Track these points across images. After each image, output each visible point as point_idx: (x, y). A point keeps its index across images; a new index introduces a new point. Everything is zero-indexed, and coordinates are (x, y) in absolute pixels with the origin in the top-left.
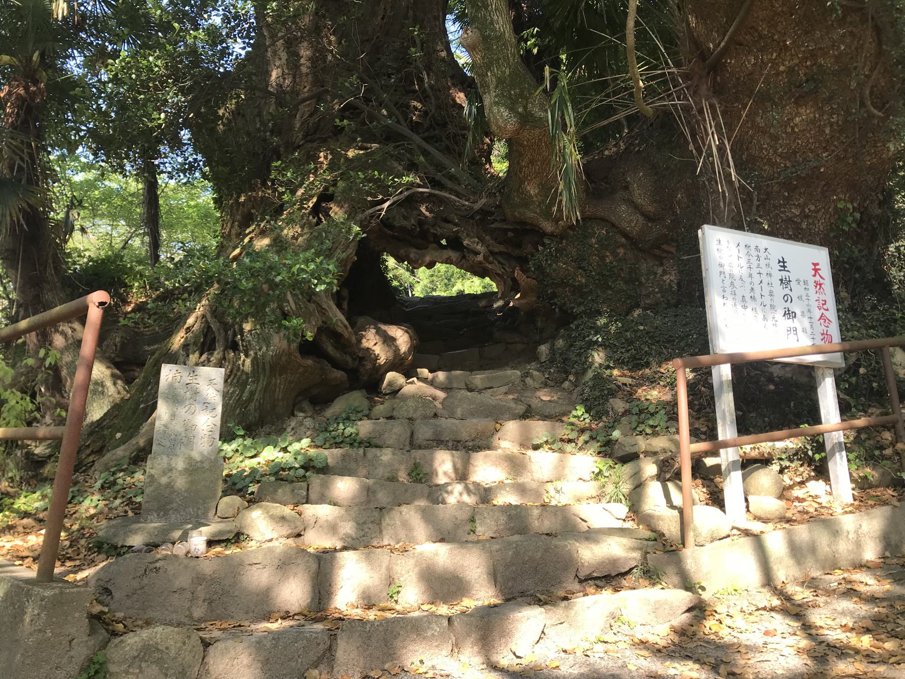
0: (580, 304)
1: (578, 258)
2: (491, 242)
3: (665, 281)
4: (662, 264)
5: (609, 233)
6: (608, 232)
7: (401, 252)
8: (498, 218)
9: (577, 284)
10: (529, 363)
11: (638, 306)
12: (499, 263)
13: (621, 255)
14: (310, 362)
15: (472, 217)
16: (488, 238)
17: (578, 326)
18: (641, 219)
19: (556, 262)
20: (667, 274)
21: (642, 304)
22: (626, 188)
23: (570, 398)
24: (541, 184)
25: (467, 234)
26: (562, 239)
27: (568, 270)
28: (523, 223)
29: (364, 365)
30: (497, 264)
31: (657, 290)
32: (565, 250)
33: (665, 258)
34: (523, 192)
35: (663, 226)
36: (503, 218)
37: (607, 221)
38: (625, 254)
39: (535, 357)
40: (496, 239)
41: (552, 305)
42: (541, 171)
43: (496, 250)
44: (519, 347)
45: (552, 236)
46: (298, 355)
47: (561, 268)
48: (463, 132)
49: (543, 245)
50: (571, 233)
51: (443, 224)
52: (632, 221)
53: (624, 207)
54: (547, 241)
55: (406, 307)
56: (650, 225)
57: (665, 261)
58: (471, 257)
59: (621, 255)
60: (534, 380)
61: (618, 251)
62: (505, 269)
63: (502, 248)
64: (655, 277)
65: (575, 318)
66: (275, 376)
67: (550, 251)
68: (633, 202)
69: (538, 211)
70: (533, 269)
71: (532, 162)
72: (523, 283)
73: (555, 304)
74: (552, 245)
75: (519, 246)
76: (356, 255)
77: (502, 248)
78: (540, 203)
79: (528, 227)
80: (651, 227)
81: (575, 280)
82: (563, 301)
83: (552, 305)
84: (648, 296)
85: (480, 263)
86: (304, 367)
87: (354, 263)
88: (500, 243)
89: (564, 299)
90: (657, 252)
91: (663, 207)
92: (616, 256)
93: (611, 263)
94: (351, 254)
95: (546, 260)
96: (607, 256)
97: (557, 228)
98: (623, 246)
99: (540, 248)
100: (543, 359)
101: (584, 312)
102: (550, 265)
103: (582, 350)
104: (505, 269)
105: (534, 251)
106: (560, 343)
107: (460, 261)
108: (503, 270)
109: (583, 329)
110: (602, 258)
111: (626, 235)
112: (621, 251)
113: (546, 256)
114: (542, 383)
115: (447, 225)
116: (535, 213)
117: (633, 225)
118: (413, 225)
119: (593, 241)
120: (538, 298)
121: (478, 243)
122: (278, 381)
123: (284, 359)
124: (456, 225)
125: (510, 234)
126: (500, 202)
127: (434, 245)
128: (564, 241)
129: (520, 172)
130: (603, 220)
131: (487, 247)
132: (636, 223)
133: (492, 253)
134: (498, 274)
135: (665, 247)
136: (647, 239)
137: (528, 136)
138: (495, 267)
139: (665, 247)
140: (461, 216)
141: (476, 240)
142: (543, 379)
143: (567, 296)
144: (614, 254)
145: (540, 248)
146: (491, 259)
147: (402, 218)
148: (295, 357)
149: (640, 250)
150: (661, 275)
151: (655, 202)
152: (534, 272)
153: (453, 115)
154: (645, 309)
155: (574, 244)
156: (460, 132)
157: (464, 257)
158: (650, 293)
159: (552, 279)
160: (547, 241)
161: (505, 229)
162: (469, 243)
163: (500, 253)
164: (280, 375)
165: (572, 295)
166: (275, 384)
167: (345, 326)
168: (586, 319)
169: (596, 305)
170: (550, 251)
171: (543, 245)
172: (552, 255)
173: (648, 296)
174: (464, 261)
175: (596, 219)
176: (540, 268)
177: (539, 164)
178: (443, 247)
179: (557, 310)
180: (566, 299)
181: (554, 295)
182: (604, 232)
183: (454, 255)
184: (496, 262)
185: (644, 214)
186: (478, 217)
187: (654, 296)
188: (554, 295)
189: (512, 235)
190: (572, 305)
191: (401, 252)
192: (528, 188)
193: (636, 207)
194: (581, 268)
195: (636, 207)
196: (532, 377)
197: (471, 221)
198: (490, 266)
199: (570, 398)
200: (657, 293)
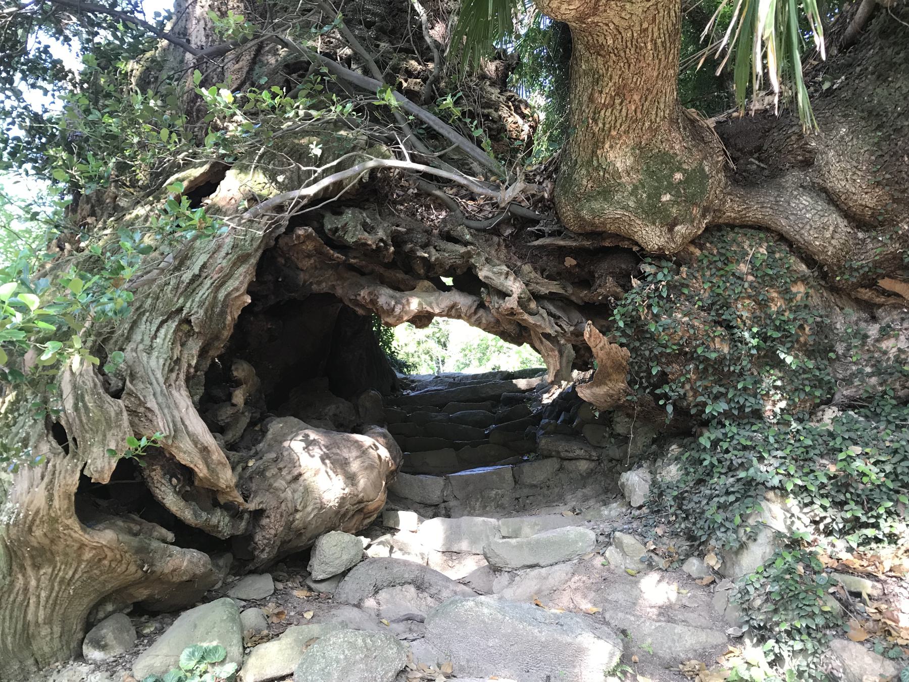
0: (717, 398)
1: (713, 304)
2: (533, 275)
3: (885, 353)
4: (874, 319)
5: (774, 252)
6: (771, 252)
7: (362, 293)
8: (546, 229)
9: (713, 356)
10: (605, 503)
11: (828, 402)
12: (550, 314)
13: (799, 297)
14: (106, 536)
15: (496, 231)
16: (527, 268)
17: (715, 443)
18: (842, 223)
19: (669, 312)
20: (889, 337)
21: (838, 397)
22: (807, 163)
23: (710, 606)
24: (638, 146)
25: (487, 259)
26: (679, 264)
27: (693, 327)
28: (596, 234)
29: (263, 528)
30: (545, 315)
31: (868, 370)
32: (687, 286)
33: (880, 306)
34: (600, 165)
35: (891, 238)
36: (556, 228)
37: (768, 229)
38: (807, 295)
39: (618, 493)
40: (543, 271)
41: (658, 397)
42: (639, 114)
43: (544, 290)
44: (583, 466)
45: (659, 257)
46: (73, 522)
47: (680, 323)
48: (486, 111)
49: (642, 277)
50: (698, 252)
51: (443, 244)
52: (825, 227)
53: (805, 200)
54: (648, 269)
55: (413, 389)
56: (860, 235)
57: (880, 312)
58: (494, 302)
59: (799, 297)
60: (624, 554)
61: (794, 289)
62: (560, 326)
63: (554, 287)
64: (864, 344)
65: (706, 424)
66: (22, 568)
67: (657, 289)
68: (824, 190)
69: (631, 204)
70: (621, 324)
71: (621, 92)
72: (601, 354)
73: (666, 396)
74: (660, 276)
75: (586, 282)
76: (249, 292)
77: (554, 287)
78: (636, 188)
79: (607, 244)
80: (864, 241)
81: (708, 347)
82: (682, 392)
83: (658, 397)
84: (848, 381)
85: (512, 312)
86: (95, 548)
87: (246, 310)
88: (550, 278)
89: (683, 387)
90: (866, 294)
91: (897, 195)
92: (791, 300)
93: (780, 313)
94: (237, 289)
95: (649, 307)
96: (773, 300)
97: (672, 239)
98: (804, 279)
99: (635, 282)
100: (637, 500)
101: (727, 414)
102: (656, 317)
103: (732, 498)
104: (560, 326)
105: (619, 290)
106: (672, 472)
107: (475, 312)
108: (558, 329)
109: (727, 451)
110: (763, 305)
111: (809, 259)
112: (799, 289)
113: (649, 297)
114: (642, 561)
115: (450, 246)
116: (626, 208)
117: (828, 235)
118: (381, 240)
119: (744, 268)
120: (631, 383)
121: (507, 274)
122: (33, 583)
123: (38, 532)
124: (466, 244)
125: (570, 262)
126: (552, 193)
127: (427, 283)
128: (684, 269)
129: (595, 121)
130: (760, 228)
131: (527, 285)
132: (835, 231)
133: (537, 297)
134: (547, 336)
135: (885, 284)
136: (856, 264)
137: (617, 20)
138: (541, 321)
139: (885, 284)
140: (478, 230)
141: (504, 268)
142: (644, 553)
143: (688, 380)
144: (786, 292)
145: (635, 282)
146: (533, 305)
147: (359, 227)
148: (67, 527)
149: (834, 289)
150: (877, 340)
151: (878, 184)
152: (623, 332)
153: (470, 87)
154: (844, 408)
155: (703, 275)
156: (480, 111)
157: (482, 305)
158: (853, 375)
159: (660, 345)
160: (648, 269)
161: (561, 248)
162: (490, 274)
163: (552, 297)
164: (37, 567)
165: (700, 379)
166: (26, 590)
167: (205, 451)
168: (735, 430)
169: (752, 400)
170: (657, 289)
171: (642, 277)
172: (660, 297)
173: (848, 381)
174: (481, 312)
175: (742, 226)
176: (634, 321)
177: (636, 97)
178: (445, 288)
179: (670, 409)
180: (688, 387)
181: (663, 378)
182: (763, 250)
183: (464, 301)
184: (542, 311)
185: (847, 215)
186: (508, 232)
187: (863, 381)
188: (663, 378)
189: (574, 262)
190: (701, 399)
191: (362, 293)
192: (611, 155)
193: (832, 199)
194: (718, 323)
195: (832, 199)
196: (620, 545)
197: (496, 239)
198: (531, 320)
199: (710, 606)
200: (870, 375)
